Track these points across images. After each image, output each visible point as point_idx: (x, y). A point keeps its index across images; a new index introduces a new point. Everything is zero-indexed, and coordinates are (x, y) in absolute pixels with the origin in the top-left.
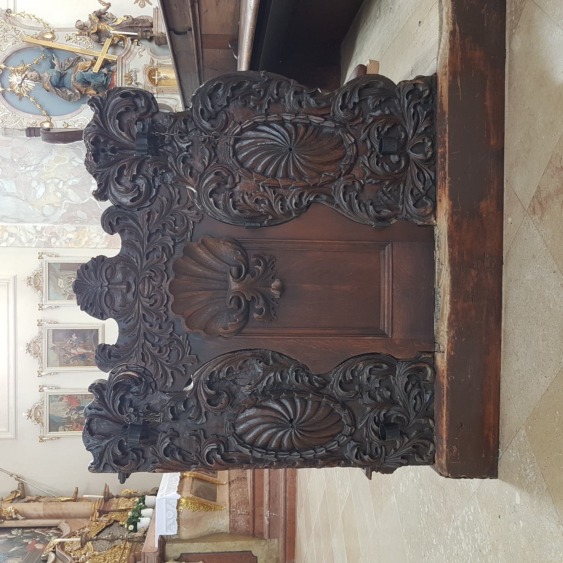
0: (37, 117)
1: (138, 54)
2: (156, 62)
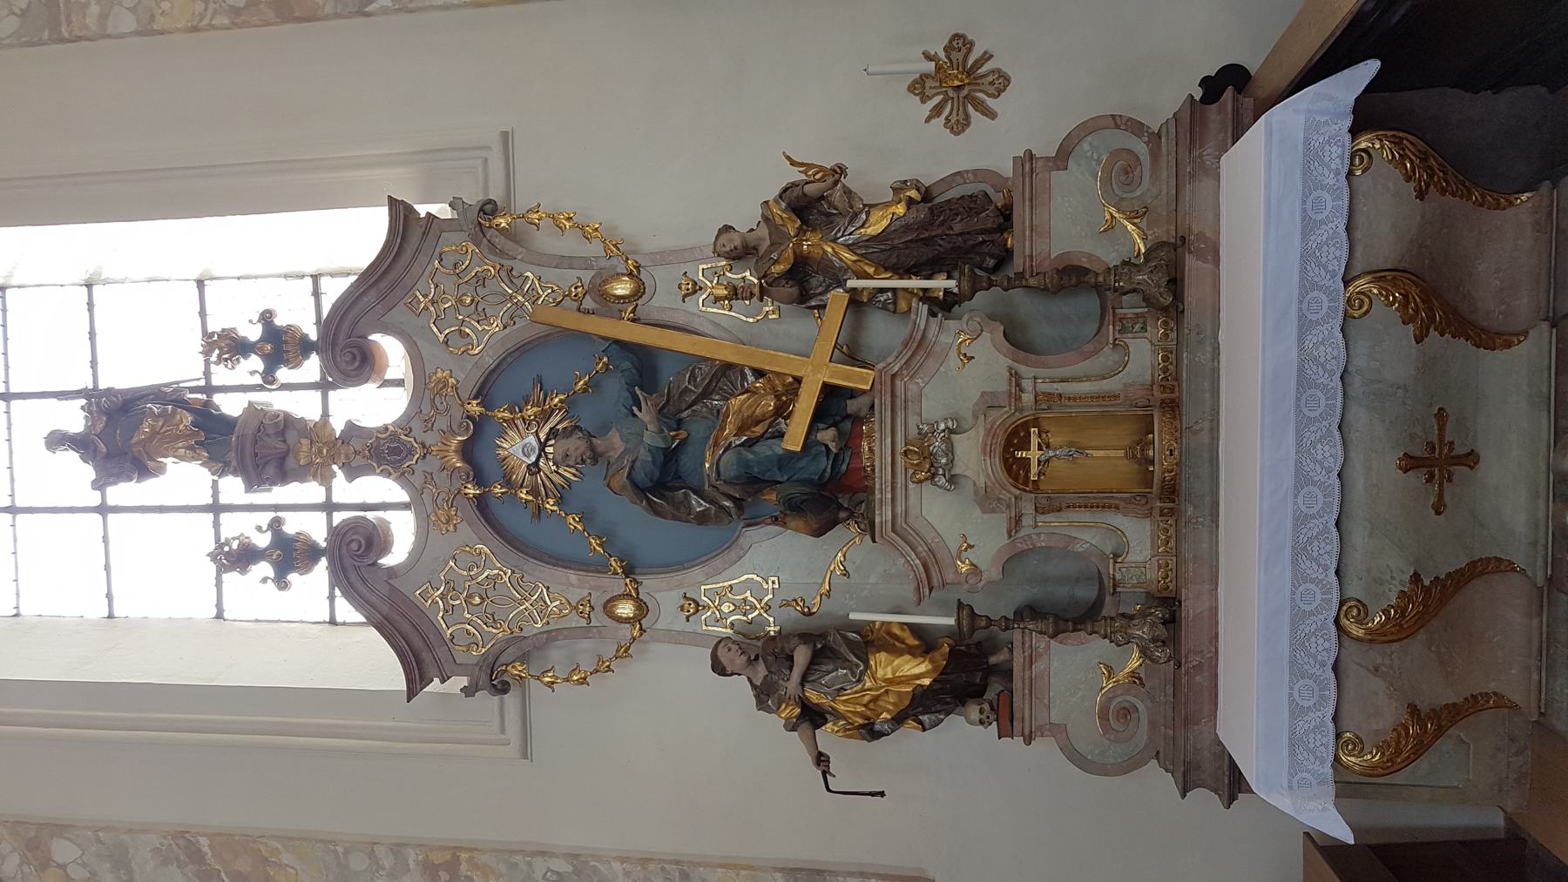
0: (593, 579)
1: (953, 354)
2: (1027, 384)
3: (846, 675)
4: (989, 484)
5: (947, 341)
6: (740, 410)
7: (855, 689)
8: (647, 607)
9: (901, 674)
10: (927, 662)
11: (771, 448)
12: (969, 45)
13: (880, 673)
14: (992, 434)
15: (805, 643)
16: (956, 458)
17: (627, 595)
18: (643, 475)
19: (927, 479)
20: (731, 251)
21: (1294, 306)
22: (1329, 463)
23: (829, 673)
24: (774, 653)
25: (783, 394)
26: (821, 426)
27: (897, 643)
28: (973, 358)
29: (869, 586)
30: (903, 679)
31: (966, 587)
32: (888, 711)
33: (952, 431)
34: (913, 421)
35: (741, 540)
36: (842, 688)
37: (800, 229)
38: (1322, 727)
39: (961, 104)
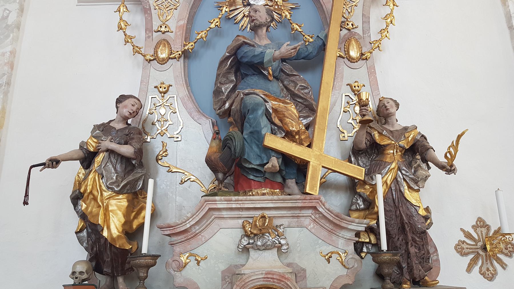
1: (331, 249)
3: (112, 179)
4: (244, 277)
5: (340, 243)
6: (288, 110)
7: (102, 185)
8: (164, 64)
9: (111, 216)
10: (118, 233)
11: (265, 126)
13: (113, 202)
14: (281, 279)
15: (135, 152)
16: (260, 252)
17: (172, 52)
18: (246, 51)
19: (246, 232)
20: (386, 107)
23: (115, 169)
24: (130, 133)
25: (300, 137)
26: (280, 160)
27: (134, 213)
28: (329, 263)
29: (174, 196)
30: (108, 218)
31: (170, 260)
32: (87, 208)
33: (279, 248)
34: (285, 222)
35: (204, 119)
36: (103, 177)
37: (403, 148)
39: (473, 250)
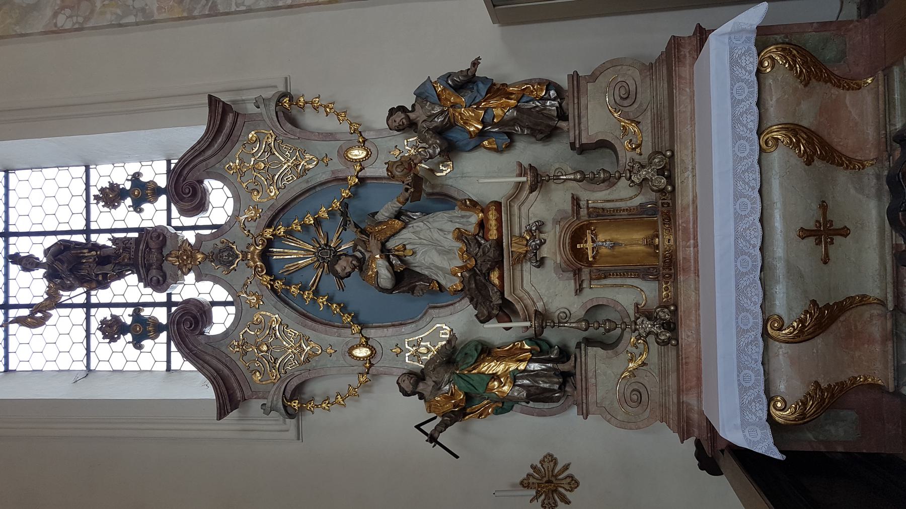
2: (583, 203)
12: (555, 461)
21: (733, 264)
22: (755, 299)
38: (756, 341)
